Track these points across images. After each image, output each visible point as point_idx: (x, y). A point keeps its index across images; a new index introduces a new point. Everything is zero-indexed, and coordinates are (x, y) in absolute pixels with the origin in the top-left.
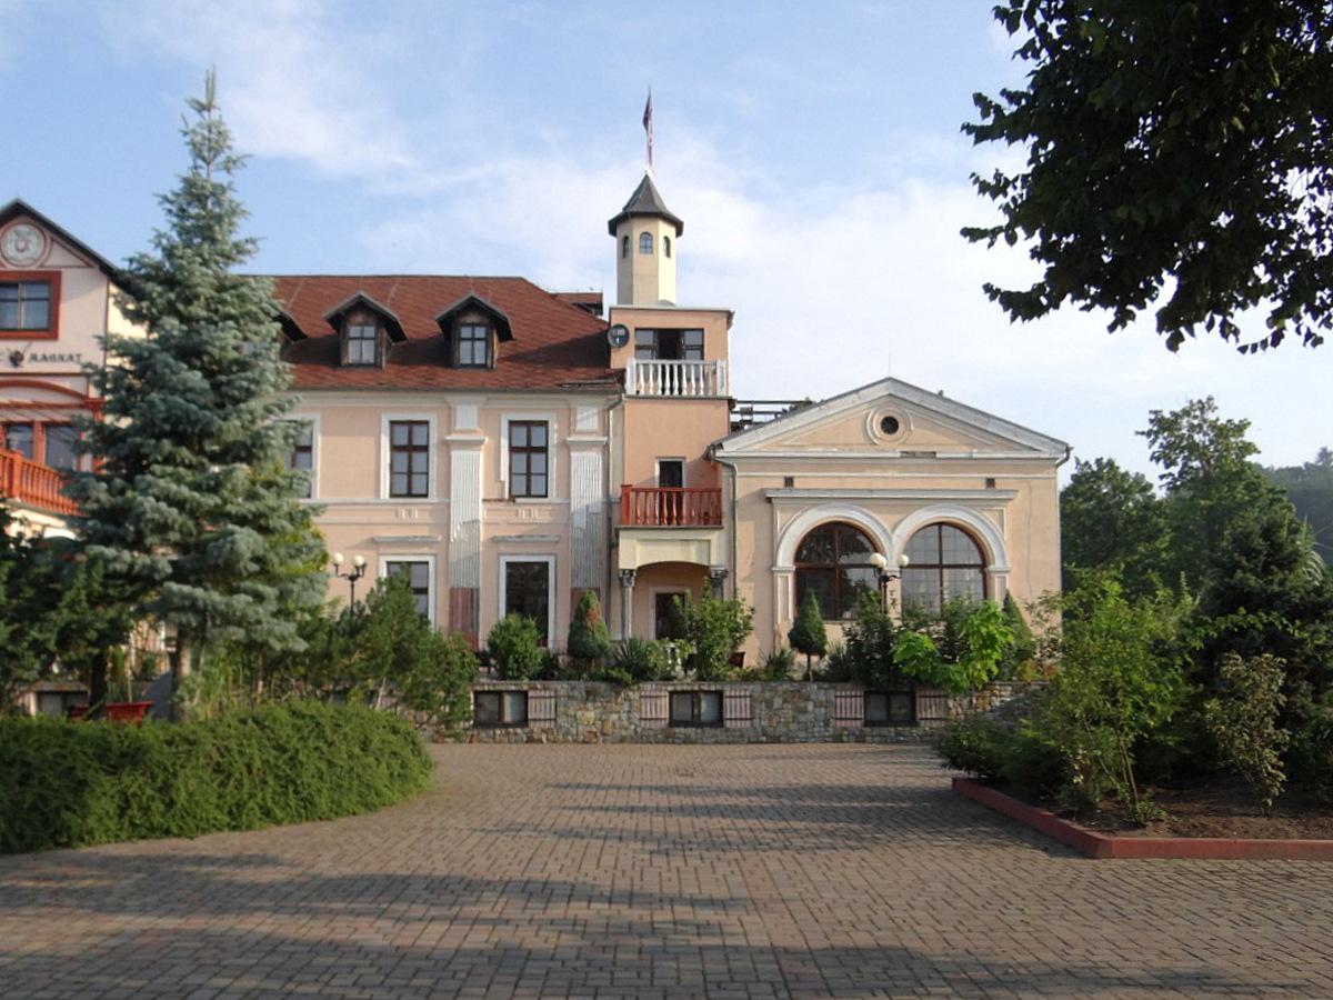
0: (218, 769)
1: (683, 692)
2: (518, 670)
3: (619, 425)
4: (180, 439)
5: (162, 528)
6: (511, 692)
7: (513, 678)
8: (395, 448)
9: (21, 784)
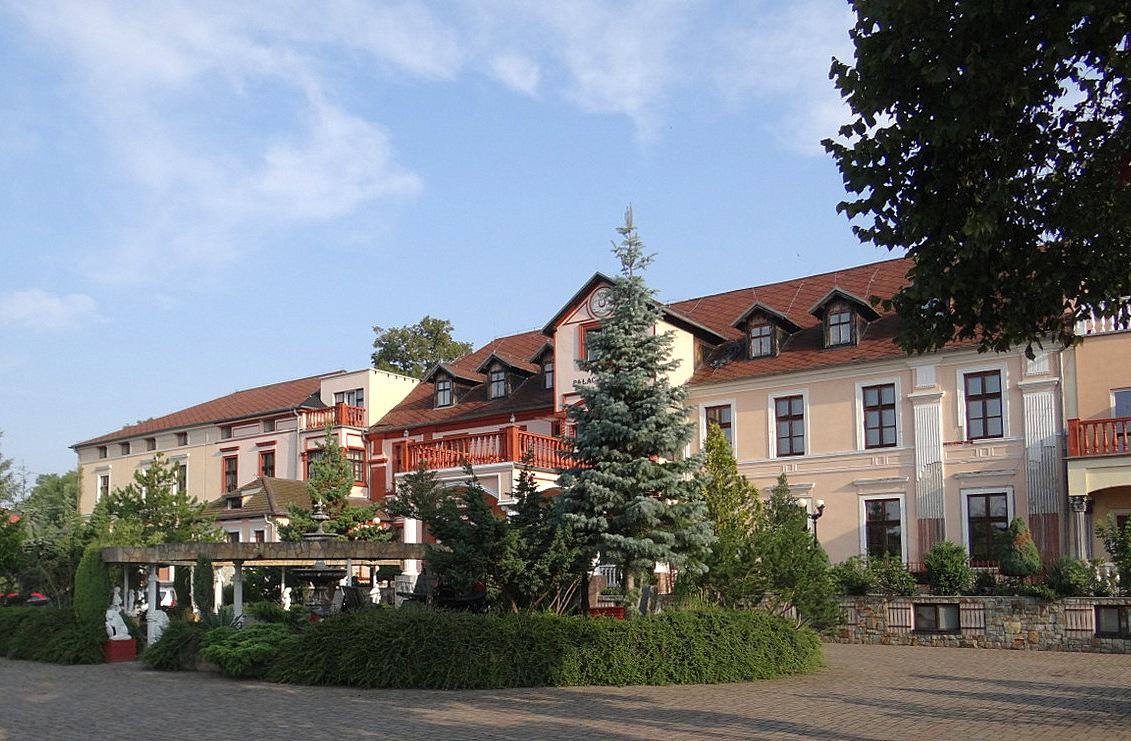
0: (640, 647)
1: (1112, 607)
2: (950, 586)
3: (1071, 365)
4: (614, 445)
5: (603, 500)
6: (944, 605)
7: (945, 593)
8: (867, 409)
9: (530, 649)
